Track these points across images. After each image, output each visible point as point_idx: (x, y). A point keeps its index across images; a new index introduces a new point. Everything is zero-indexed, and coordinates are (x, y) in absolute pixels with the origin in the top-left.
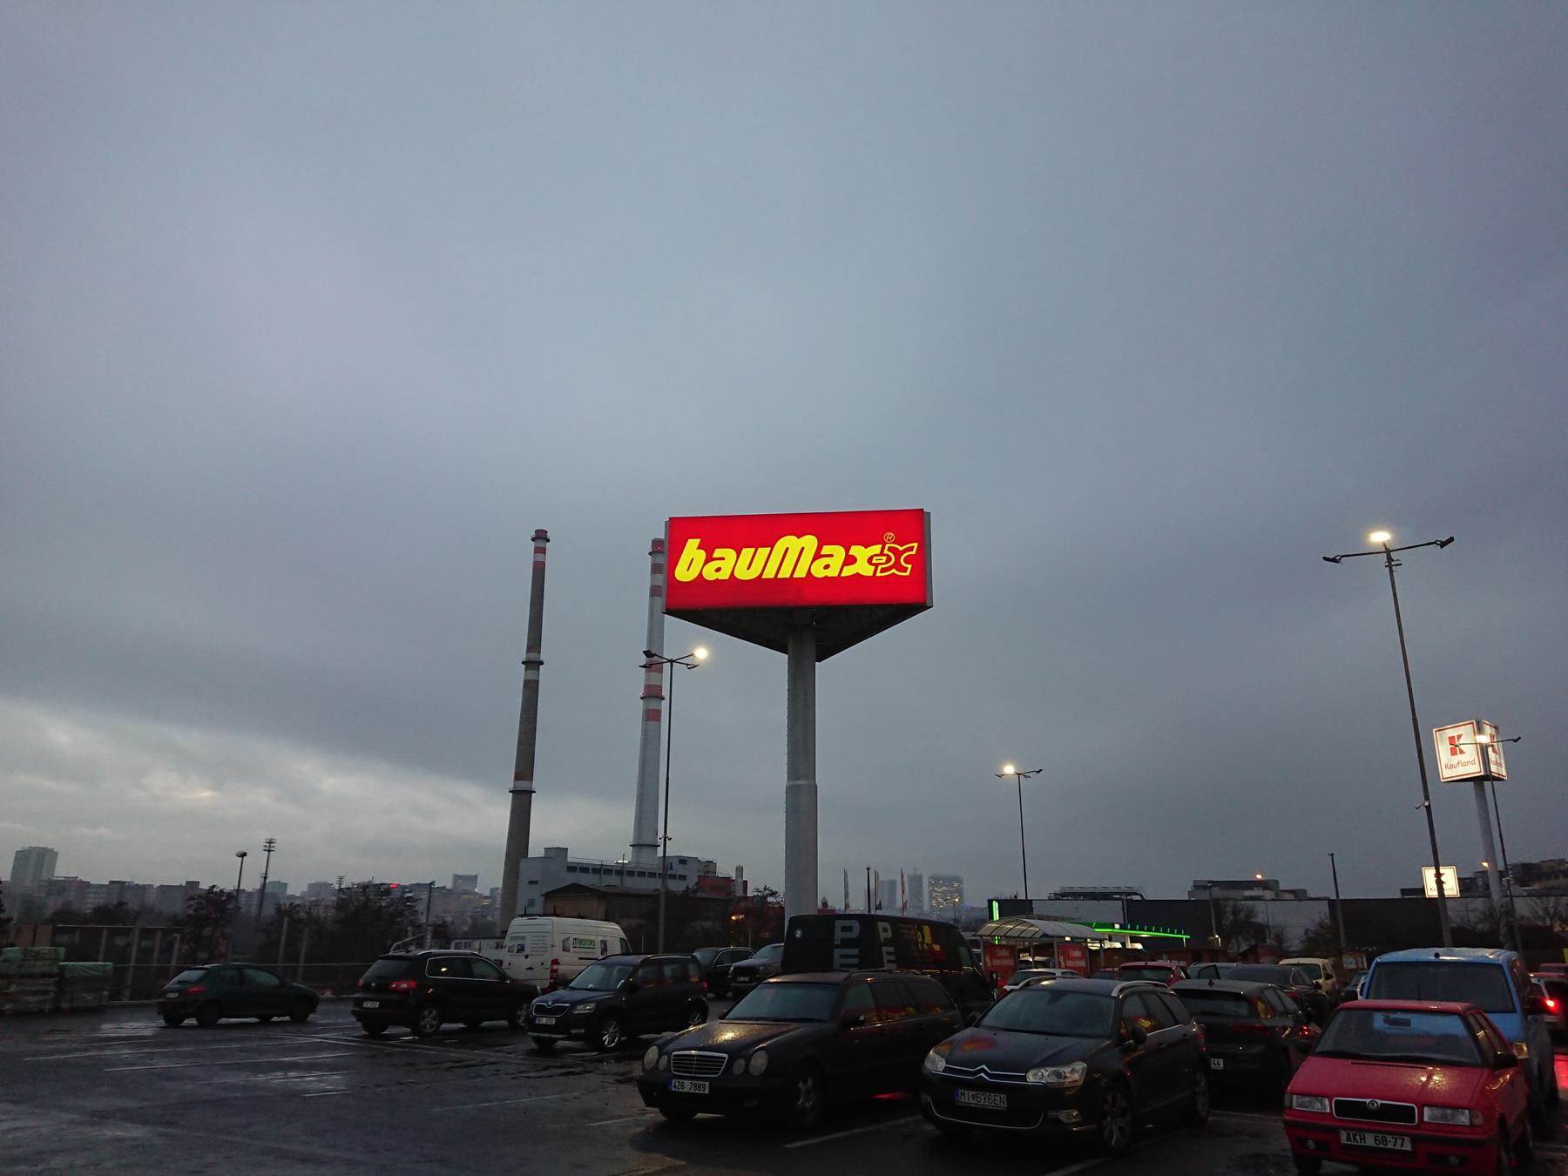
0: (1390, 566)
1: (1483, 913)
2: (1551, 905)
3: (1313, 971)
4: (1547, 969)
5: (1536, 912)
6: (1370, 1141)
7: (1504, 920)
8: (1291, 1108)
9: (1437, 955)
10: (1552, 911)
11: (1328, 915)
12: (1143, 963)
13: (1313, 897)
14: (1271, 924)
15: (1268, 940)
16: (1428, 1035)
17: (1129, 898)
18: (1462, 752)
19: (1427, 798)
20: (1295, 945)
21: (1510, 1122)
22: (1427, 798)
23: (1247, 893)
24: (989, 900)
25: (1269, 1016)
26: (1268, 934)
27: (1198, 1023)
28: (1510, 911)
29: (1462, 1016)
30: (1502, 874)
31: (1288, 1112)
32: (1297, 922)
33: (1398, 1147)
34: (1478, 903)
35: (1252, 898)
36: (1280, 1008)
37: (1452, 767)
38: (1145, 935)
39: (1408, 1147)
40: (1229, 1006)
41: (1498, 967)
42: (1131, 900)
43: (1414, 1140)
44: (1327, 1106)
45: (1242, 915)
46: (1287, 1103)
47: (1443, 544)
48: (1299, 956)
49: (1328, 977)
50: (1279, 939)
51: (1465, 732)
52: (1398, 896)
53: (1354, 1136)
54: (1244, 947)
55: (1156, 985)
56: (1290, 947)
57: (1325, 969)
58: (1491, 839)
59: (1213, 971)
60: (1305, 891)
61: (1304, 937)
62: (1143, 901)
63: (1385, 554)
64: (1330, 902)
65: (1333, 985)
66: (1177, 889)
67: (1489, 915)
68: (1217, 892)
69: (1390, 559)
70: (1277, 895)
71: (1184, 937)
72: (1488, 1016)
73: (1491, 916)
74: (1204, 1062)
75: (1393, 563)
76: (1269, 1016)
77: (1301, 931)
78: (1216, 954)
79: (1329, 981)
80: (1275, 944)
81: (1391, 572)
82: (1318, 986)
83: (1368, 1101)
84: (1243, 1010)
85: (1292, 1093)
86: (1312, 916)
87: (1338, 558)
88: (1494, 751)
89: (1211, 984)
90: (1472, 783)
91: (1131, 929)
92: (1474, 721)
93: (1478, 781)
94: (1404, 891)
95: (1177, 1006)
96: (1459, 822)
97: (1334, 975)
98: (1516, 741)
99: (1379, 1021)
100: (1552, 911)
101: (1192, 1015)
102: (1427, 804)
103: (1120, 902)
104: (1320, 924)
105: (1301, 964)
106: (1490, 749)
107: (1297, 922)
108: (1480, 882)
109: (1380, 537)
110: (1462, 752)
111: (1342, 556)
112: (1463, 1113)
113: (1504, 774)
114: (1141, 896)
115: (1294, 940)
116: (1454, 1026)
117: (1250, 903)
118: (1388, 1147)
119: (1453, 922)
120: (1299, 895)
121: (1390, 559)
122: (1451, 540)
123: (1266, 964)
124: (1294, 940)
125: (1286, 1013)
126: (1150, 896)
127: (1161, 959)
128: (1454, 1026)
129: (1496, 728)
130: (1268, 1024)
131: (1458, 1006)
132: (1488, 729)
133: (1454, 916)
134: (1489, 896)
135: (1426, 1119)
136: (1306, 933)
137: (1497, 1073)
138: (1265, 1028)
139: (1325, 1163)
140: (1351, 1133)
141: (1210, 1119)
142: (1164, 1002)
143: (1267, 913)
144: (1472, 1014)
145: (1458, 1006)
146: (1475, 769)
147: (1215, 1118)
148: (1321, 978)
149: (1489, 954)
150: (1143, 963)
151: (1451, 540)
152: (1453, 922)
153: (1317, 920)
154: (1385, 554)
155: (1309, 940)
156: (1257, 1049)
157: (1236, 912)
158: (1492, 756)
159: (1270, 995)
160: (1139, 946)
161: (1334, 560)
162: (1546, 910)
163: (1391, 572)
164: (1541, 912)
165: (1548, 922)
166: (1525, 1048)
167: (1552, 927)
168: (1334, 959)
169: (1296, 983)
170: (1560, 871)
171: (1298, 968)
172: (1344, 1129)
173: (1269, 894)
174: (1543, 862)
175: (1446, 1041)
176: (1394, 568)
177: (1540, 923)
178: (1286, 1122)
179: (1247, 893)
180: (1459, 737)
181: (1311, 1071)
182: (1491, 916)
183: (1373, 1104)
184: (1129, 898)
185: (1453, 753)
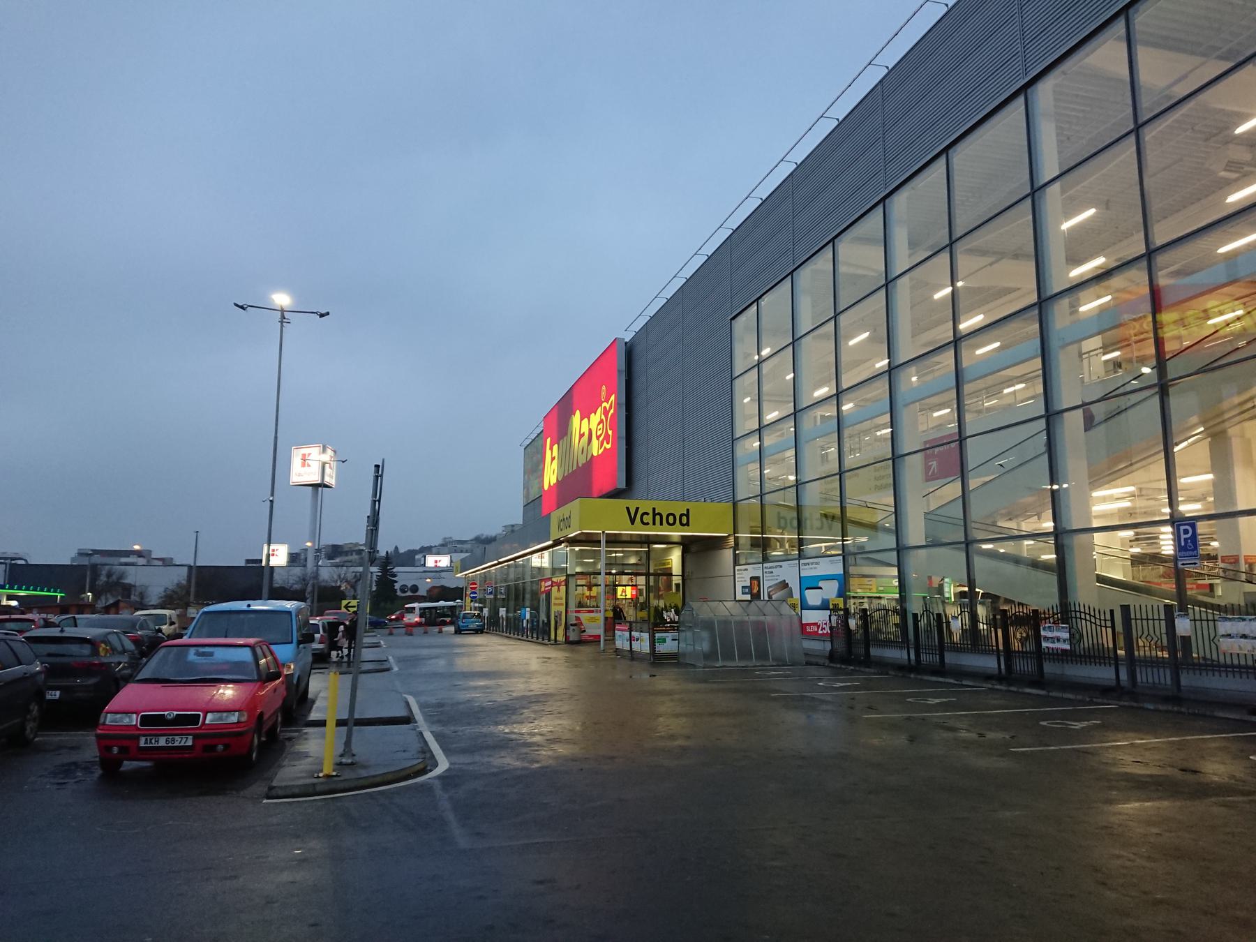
0: (282, 322)
1: (299, 577)
2: (343, 572)
3: (161, 619)
4: (328, 614)
5: (333, 577)
6: (162, 742)
7: (311, 582)
8: (104, 724)
9: (249, 606)
10: (342, 576)
11: (186, 578)
12: (7, 617)
13: (178, 563)
14: (137, 584)
15: (132, 597)
16: (227, 663)
17: (13, 562)
18: (309, 466)
19: (272, 495)
20: (154, 600)
21: (265, 717)
22: (272, 495)
23: (124, 560)
24: (688, 525)
25: (108, 655)
26: (133, 593)
27: (42, 663)
28: (316, 576)
29: (252, 647)
30: (318, 551)
31: (101, 727)
32: (157, 582)
33: (182, 744)
34: (297, 571)
35: (126, 564)
36: (120, 648)
37: (300, 475)
38: (22, 593)
39: (190, 743)
40: (74, 648)
41: (289, 613)
42: (16, 564)
43: (196, 737)
44: (134, 720)
45: (114, 578)
46: (102, 720)
47: (322, 316)
48: (155, 607)
49: (172, 623)
50: (142, 595)
51: (314, 453)
52: (243, 564)
53: (151, 740)
54: (111, 601)
55: (7, 634)
56: (149, 601)
57: (170, 618)
58: (316, 530)
59: (72, 621)
60: (172, 559)
61: (163, 594)
62: (28, 566)
63: (280, 312)
64: (190, 567)
65: (175, 629)
66: (62, 556)
67: (303, 579)
68: (97, 559)
69: (283, 317)
70: (148, 561)
71: (59, 595)
72: (273, 647)
73: (304, 580)
74: (40, 694)
75: (284, 320)
76: (108, 655)
77: (162, 589)
78: (82, 608)
79: (173, 627)
80: (138, 599)
81: (282, 326)
82: (160, 630)
83: (166, 713)
84: (86, 650)
85: (107, 713)
86: (176, 577)
87: (245, 306)
88: (330, 468)
89: (62, 631)
90: (311, 488)
91: (9, 589)
92: (321, 445)
93: (315, 486)
94: (248, 561)
95: (24, 651)
96: (295, 513)
97: (177, 623)
98: (343, 462)
99: (192, 655)
100: (342, 576)
101: (37, 657)
102: (271, 499)
103: (4, 566)
104: (177, 584)
105: (152, 615)
106: (327, 466)
107: (157, 582)
108: (302, 557)
109: (282, 299)
110: (309, 466)
111: (249, 306)
112: (234, 714)
113: (333, 483)
114: (26, 560)
115: (155, 595)
116: (245, 655)
117: (123, 567)
118: (160, 745)
119: (277, 583)
120: (167, 562)
121: (283, 317)
122: (328, 314)
123: (125, 615)
124: (155, 595)
125: (124, 651)
126: (34, 560)
127: (31, 613)
128: (245, 655)
129: (335, 452)
130: (105, 660)
131: (252, 641)
132: (330, 452)
133: (278, 580)
134: (305, 566)
135: (207, 722)
136: (165, 591)
137: (266, 684)
138: (102, 665)
139: (125, 762)
140: (149, 738)
141: (37, 739)
142: (12, 650)
143: (135, 576)
144: (260, 646)
145: (252, 641)
146: (316, 479)
147: (41, 739)
148: (166, 624)
149: (289, 605)
150: (7, 617)
151: (328, 314)
152: (277, 583)
153: (176, 581)
154: (280, 312)
155: (166, 596)
156: (92, 681)
157: (109, 575)
158: (328, 470)
159: (113, 639)
160: (14, 603)
161: (242, 307)
162: (339, 576)
163: (282, 326)
164: (336, 577)
165: (338, 584)
166: (292, 667)
167: (340, 587)
168: (181, 610)
169: (142, 628)
170: (354, 551)
171: (146, 618)
172: (144, 735)
173: (141, 561)
174: (346, 544)
175: (238, 666)
176: (284, 324)
177: (333, 584)
178: (98, 737)
179: (124, 560)
180: (309, 454)
181: (130, 695)
182: (304, 580)
183: (170, 715)
184: (13, 562)
185: (303, 465)
